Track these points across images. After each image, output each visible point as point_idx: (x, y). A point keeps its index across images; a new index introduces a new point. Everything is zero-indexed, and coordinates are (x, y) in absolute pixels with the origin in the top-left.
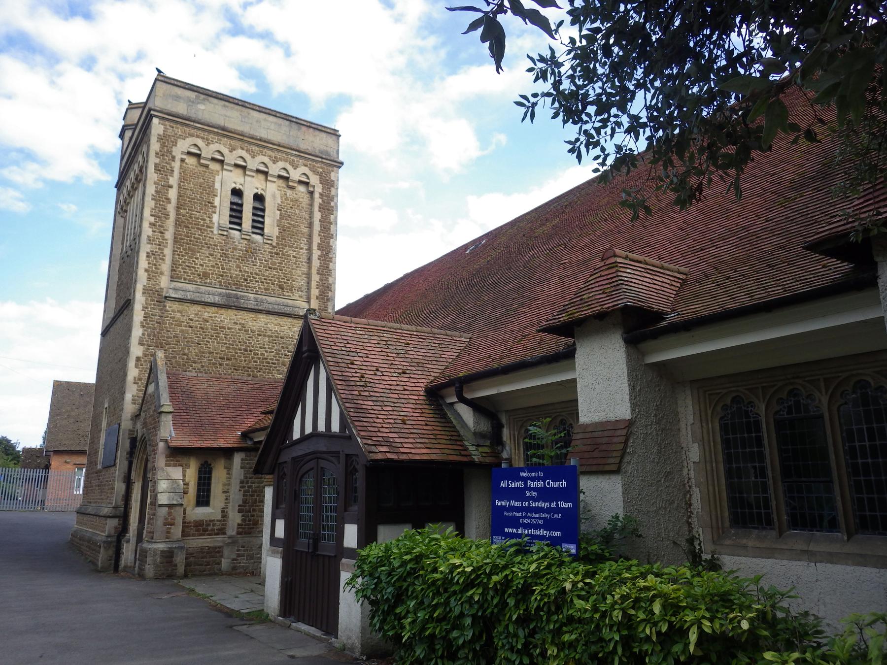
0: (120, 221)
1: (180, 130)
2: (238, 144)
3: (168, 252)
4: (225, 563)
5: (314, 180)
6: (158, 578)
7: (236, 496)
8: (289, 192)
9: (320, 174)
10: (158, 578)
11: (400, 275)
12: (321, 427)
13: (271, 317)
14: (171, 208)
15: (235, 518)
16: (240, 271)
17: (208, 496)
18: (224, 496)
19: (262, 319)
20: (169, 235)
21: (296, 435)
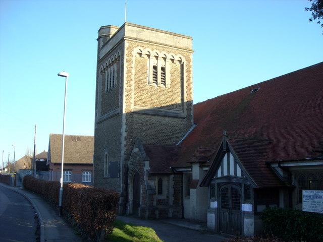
0: (101, 76)
1: (134, 44)
2: (155, 47)
3: (133, 94)
4: (170, 215)
5: (184, 60)
6: (149, 218)
7: (172, 191)
8: (174, 65)
9: (185, 57)
10: (149, 218)
11: (216, 96)
12: (232, 173)
13: (171, 118)
14: (133, 77)
15: (172, 199)
16: (104, 69)
17: (162, 191)
18: (167, 191)
19: (167, 119)
20: (133, 87)
21: (219, 175)
